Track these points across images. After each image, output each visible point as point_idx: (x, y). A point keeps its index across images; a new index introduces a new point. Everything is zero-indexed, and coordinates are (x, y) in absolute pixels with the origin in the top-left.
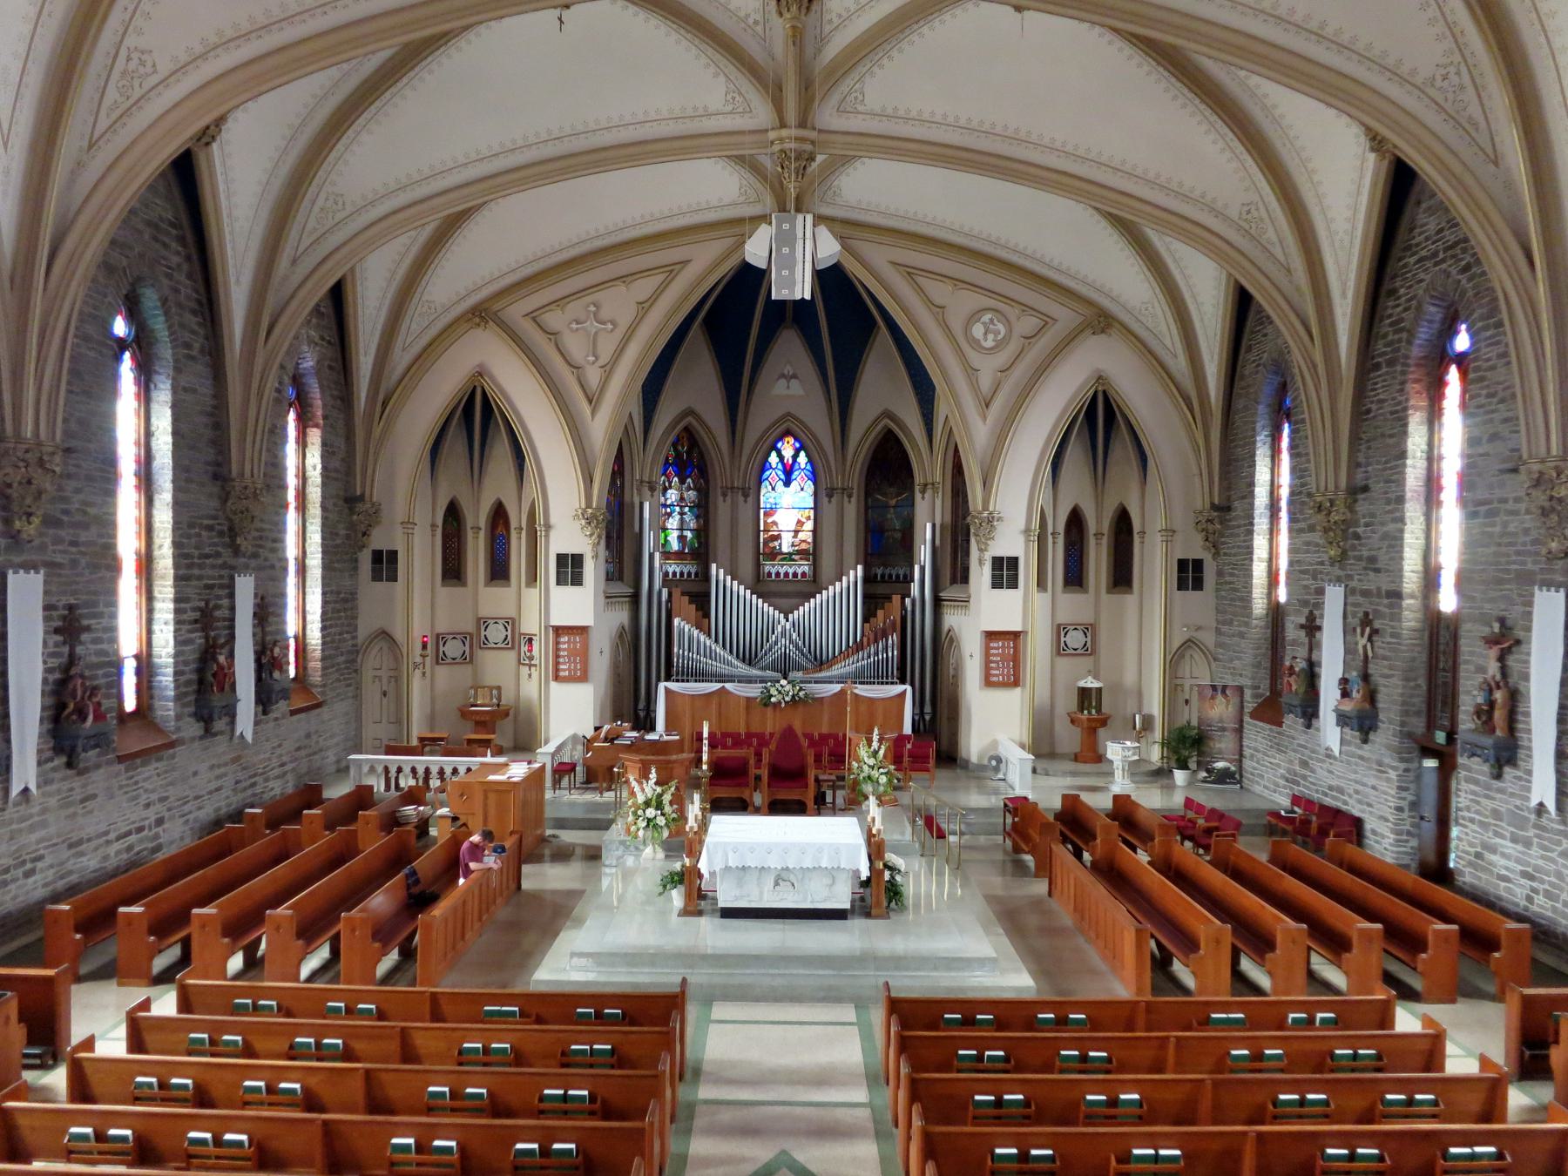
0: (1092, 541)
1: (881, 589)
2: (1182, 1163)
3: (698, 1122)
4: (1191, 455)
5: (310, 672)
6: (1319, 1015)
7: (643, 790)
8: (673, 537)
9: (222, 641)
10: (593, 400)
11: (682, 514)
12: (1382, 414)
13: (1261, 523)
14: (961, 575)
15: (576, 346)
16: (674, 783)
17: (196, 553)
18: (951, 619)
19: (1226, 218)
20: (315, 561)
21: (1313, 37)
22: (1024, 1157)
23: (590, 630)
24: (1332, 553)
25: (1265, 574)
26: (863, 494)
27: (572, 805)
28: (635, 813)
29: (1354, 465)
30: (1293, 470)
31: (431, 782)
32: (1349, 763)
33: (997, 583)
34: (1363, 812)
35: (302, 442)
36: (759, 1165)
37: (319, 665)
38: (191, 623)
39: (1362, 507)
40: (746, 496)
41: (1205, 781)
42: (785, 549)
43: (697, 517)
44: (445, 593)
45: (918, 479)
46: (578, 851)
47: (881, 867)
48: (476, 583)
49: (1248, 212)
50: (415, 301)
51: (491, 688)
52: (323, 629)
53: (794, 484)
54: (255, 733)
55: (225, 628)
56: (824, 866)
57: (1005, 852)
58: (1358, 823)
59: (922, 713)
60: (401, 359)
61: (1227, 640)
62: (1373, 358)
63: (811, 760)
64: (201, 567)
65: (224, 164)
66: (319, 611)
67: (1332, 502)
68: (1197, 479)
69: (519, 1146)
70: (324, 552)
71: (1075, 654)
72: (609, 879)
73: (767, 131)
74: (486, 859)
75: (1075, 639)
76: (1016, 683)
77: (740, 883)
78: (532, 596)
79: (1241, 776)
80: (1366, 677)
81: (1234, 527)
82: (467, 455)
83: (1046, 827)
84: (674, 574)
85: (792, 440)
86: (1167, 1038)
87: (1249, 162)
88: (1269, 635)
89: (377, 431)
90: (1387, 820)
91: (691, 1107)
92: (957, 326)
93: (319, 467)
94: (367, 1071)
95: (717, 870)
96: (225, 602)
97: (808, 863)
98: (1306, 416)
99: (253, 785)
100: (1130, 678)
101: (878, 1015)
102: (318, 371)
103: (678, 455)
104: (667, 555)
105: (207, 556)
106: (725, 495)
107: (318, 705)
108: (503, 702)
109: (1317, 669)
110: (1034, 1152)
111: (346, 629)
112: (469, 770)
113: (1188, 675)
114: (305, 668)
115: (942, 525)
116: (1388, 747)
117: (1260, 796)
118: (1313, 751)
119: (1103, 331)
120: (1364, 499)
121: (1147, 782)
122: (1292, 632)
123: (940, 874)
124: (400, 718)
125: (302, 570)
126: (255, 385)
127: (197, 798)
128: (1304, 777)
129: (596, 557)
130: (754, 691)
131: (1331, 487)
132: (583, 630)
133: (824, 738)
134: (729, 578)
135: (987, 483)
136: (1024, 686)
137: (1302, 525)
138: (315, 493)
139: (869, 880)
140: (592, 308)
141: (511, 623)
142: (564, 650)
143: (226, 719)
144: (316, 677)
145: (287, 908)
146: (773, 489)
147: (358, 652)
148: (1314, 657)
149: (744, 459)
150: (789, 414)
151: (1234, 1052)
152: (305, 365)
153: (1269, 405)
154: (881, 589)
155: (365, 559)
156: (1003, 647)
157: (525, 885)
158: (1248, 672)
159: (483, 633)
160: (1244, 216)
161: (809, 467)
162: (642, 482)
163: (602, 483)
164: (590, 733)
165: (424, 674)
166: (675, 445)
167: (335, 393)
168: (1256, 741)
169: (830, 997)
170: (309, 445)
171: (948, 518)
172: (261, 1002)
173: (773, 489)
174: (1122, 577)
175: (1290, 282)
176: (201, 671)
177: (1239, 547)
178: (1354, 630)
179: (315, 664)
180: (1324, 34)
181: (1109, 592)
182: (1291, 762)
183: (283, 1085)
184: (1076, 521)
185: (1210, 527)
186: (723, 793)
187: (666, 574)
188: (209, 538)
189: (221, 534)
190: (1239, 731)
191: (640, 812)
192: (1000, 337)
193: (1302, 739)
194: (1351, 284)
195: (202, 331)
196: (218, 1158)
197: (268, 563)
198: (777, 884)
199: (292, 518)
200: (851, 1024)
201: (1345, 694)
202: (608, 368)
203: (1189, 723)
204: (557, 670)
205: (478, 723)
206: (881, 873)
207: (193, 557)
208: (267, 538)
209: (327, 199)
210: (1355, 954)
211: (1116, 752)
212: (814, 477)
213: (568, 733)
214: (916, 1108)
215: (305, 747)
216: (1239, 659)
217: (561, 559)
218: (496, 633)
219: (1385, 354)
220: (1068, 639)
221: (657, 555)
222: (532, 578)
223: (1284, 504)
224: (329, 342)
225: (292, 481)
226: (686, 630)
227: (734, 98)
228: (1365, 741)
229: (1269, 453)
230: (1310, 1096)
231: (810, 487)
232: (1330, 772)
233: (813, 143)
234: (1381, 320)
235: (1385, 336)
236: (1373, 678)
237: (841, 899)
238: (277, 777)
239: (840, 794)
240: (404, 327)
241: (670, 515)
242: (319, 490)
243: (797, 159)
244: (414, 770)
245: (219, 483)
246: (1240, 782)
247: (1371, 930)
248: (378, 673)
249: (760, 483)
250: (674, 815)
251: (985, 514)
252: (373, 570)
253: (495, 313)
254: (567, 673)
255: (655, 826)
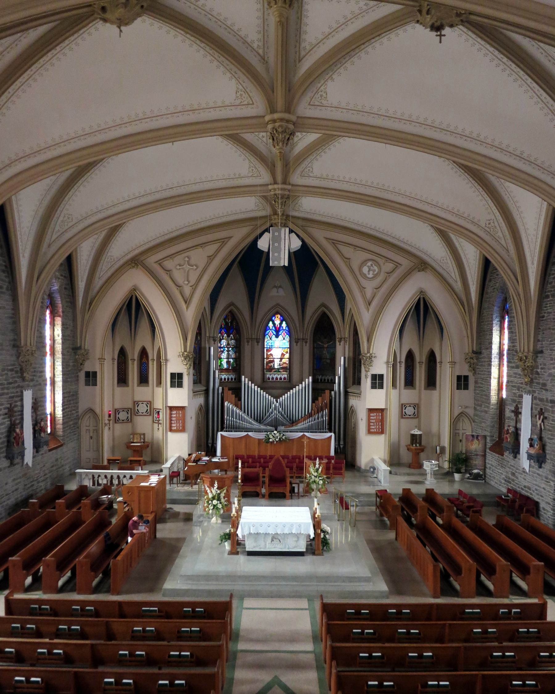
0: (418, 366)
1: (321, 386)
2: (450, 688)
3: (239, 662)
4: (464, 329)
5: (57, 430)
6: (514, 610)
7: (211, 492)
8: (224, 362)
9: (18, 421)
10: (187, 302)
11: (228, 351)
12: (549, 319)
13: (495, 362)
14: (357, 382)
15: (179, 276)
16: (225, 488)
17: (6, 382)
18: (352, 401)
19: (479, 226)
20: (59, 379)
21: (518, 158)
22: (381, 685)
23: (186, 409)
24: (526, 380)
25: (496, 385)
26: (312, 342)
27: (179, 492)
28: (208, 502)
29: (536, 341)
30: (510, 339)
31: (114, 481)
32: (533, 476)
33: (374, 386)
34: (539, 499)
35: (53, 324)
36: (265, 683)
37: (61, 427)
38: (4, 415)
39: (540, 360)
40: (258, 342)
41: (468, 478)
42: (276, 367)
43: (235, 352)
44: (119, 390)
45: (338, 335)
46: (181, 516)
47: (319, 532)
48: (133, 386)
49: (489, 224)
50: (104, 256)
51: (140, 434)
52: (63, 410)
53: (280, 337)
54: (33, 462)
55: (19, 415)
56: (294, 532)
57: (377, 515)
58: (537, 504)
59: (339, 444)
60: (98, 283)
61: (479, 413)
62: (546, 292)
63: (288, 474)
64: (8, 389)
65: (17, 204)
66: (61, 402)
67: (526, 357)
68: (466, 339)
69: (160, 682)
70: (63, 375)
71: (410, 417)
72: (198, 533)
73: (268, 185)
74: (140, 528)
75: (410, 411)
76: (382, 432)
77: (256, 541)
78: (159, 391)
79: (485, 476)
80: (541, 439)
81: (482, 362)
82: (129, 325)
83: (395, 507)
84: (225, 379)
85: (279, 316)
86: (445, 624)
87: (492, 205)
88: (498, 412)
89: (87, 317)
90: (549, 504)
91: (235, 653)
92: (355, 268)
93: (61, 335)
94: (92, 646)
95: (246, 534)
96: (19, 403)
97: (286, 531)
98: (515, 315)
99: (32, 485)
100: (435, 429)
101: (317, 606)
102: (60, 291)
103: (227, 323)
104: (221, 370)
105: (11, 383)
106: (248, 342)
107: (61, 445)
108: (146, 440)
109: (519, 432)
110: (385, 683)
111: (73, 408)
112: (131, 477)
113: (461, 428)
114: (55, 428)
115: (349, 358)
116: (550, 471)
117: (493, 486)
118: (517, 469)
119: (423, 270)
120: (541, 357)
121: (441, 478)
122: (508, 413)
123: (347, 530)
124: (99, 449)
125: (53, 383)
126: (32, 303)
127: (7, 495)
128: (513, 480)
129: (188, 374)
130: (261, 436)
131: (526, 350)
132: (182, 408)
133: (294, 458)
134: (250, 382)
135: (369, 340)
136: (386, 434)
137: (513, 365)
138: (59, 347)
139: (314, 538)
140: (187, 259)
141: (150, 403)
142: (174, 417)
143: (20, 457)
144: (60, 432)
145: (51, 557)
146: (271, 339)
147: (79, 419)
148: (518, 426)
149: (257, 326)
150: (278, 304)
151: (475, 630)
152: (54, 288)
153: (499, 307)
154: (321, 386)
155: (82, 375)
156: (376, 416)
157: (159, 535)
158: (489, 429)
159: (136, 408)
160: (488, 226)
161: (287, 329)
162: (210, 337)
163: (191, 340)
164: (186, 457)
165: (109, 428)
166: (225, 319)
167: (68, 300)
168: (492, 461)
169: (297, 596)
170: (56, 325)
171: (351, 355)
172: (43, 607)
173: (271, 339)
174: (431, 382)
175: (508, 256)
176: (8, 436)
177: (485, 371)
178: (536, 416)
179: (59, 426)
180: (522, 156)
181: (425, 389)
182: (507, 472)
183: (55, 651)
184: (410, 356)
185: (472, 361)
186: (248, 489)
187: (221, 379)
188: (11, 375)
189: (17, 372)
190: (484, 456)
191: (210, 502)
192: (375, 273)
193: (512, 462)
194: (536, 258)
195: (7, 280)
196: (28, 688)
197: (37, 383)
198: (272, 540)
199: (48, 359)
200: (306, 609)
201: (531, 445)
202: (194, 287)
203: (461, 452)
204: (171, 427)
205: (134, 451)
206: (320, 534)
207: (4, 385)
208: (37, 372)
209: (64, 217)
210: (531, 577)
211: (429, 466)
212: (290, 333)
213: (177, 455)
214: (334, 663)
215: (55, 466)
216: (485, 422)
217: (173, 375)
218: (142, 408)
219: (551, 291)
220: (406, 411)
221: (217, 371)
222: (159, 383)
223: (505, 353)
224: (65, 277)
225: (48, 342)
226: (231, 407)
227: (252, 170)
228: (540, 467)
229: (499, 329)
230: (507, 654)
231: (287, 338)
232: (525, 479)
233: (289, 191)
234: (550, 275)
235: (551, 283)
236: (544, 439)
237: (302, 548)
238: (43, 481)
239: (302, 486)
240: (99, 269)
241: (223, 352)
242: (61, 346)
243: (282, 198)
244: (106, 477)
245: (15, 349)
246: (484, 479)
247: (539, 565)
248: (87, 428)
249: (265, 336)
250: (226, 503)
251: (368, 355)
252: (86, 381)
253: (142, 261)
254: (175, 428)
255: (217, 508)
